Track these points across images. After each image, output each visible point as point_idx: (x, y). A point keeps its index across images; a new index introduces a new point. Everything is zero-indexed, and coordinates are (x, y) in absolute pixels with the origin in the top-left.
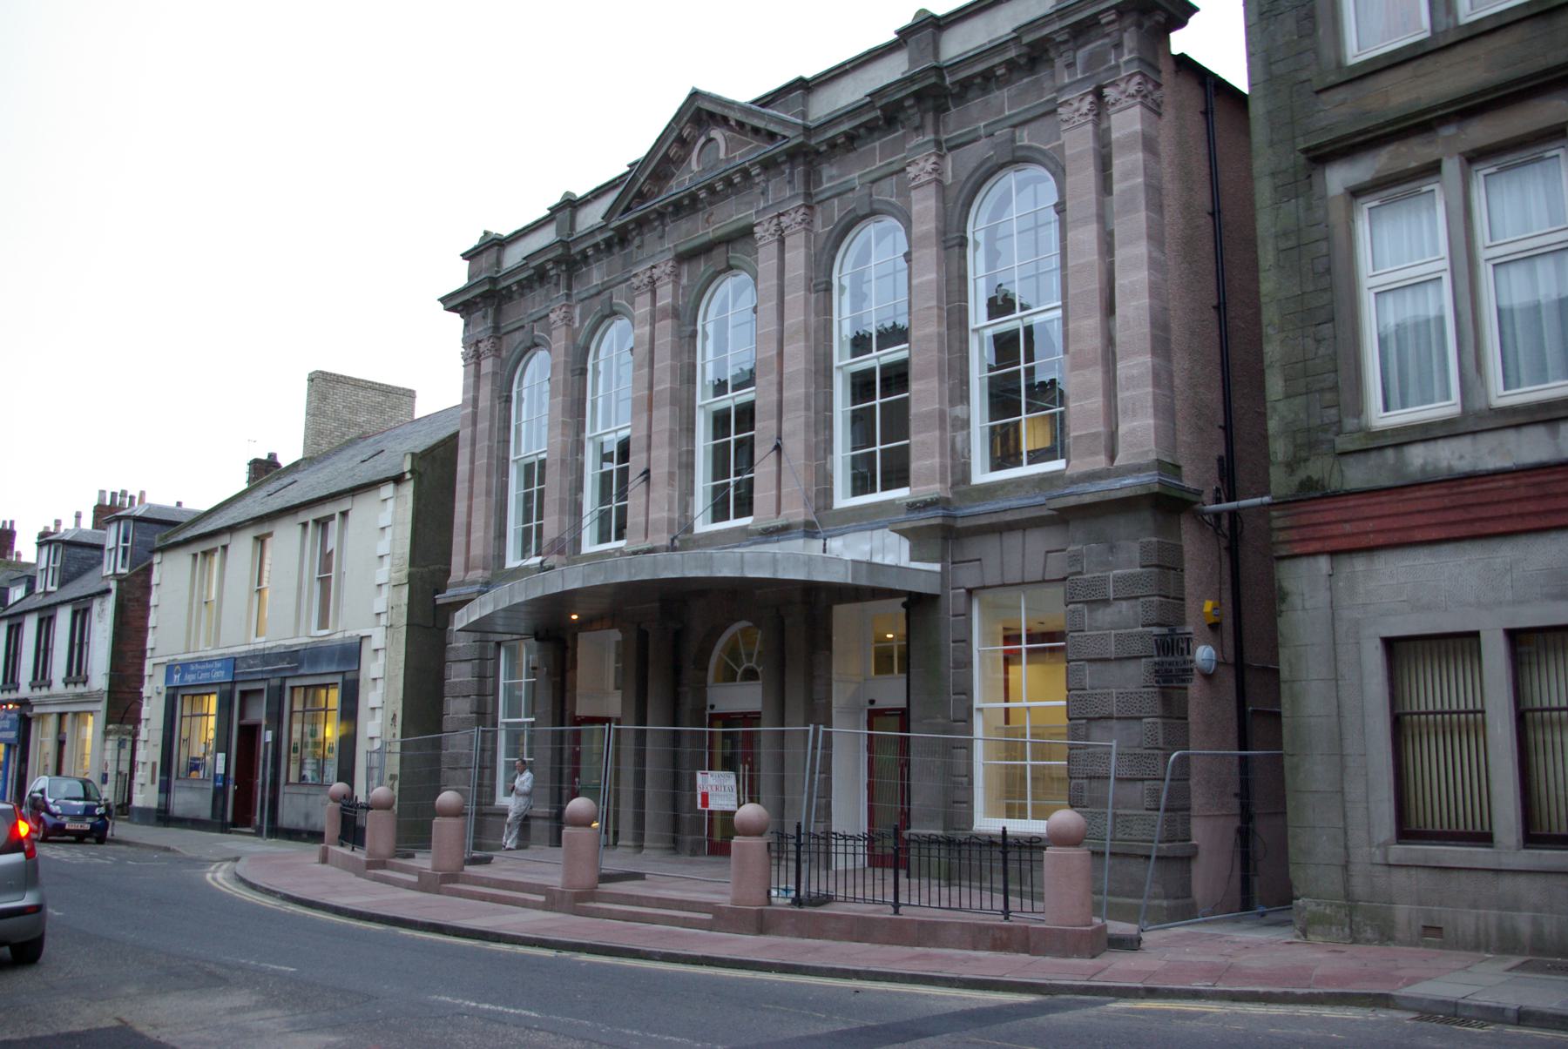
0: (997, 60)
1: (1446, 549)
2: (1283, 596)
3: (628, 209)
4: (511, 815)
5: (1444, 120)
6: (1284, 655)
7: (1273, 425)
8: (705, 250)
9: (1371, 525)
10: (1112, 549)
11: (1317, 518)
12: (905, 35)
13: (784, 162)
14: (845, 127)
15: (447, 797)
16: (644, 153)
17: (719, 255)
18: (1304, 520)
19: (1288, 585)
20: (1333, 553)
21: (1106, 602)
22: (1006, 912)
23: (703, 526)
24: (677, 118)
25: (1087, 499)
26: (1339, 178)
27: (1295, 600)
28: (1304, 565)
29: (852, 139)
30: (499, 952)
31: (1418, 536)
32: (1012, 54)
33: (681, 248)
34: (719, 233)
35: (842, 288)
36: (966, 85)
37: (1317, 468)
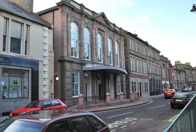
23: (102, 62)
26: (130, 55)
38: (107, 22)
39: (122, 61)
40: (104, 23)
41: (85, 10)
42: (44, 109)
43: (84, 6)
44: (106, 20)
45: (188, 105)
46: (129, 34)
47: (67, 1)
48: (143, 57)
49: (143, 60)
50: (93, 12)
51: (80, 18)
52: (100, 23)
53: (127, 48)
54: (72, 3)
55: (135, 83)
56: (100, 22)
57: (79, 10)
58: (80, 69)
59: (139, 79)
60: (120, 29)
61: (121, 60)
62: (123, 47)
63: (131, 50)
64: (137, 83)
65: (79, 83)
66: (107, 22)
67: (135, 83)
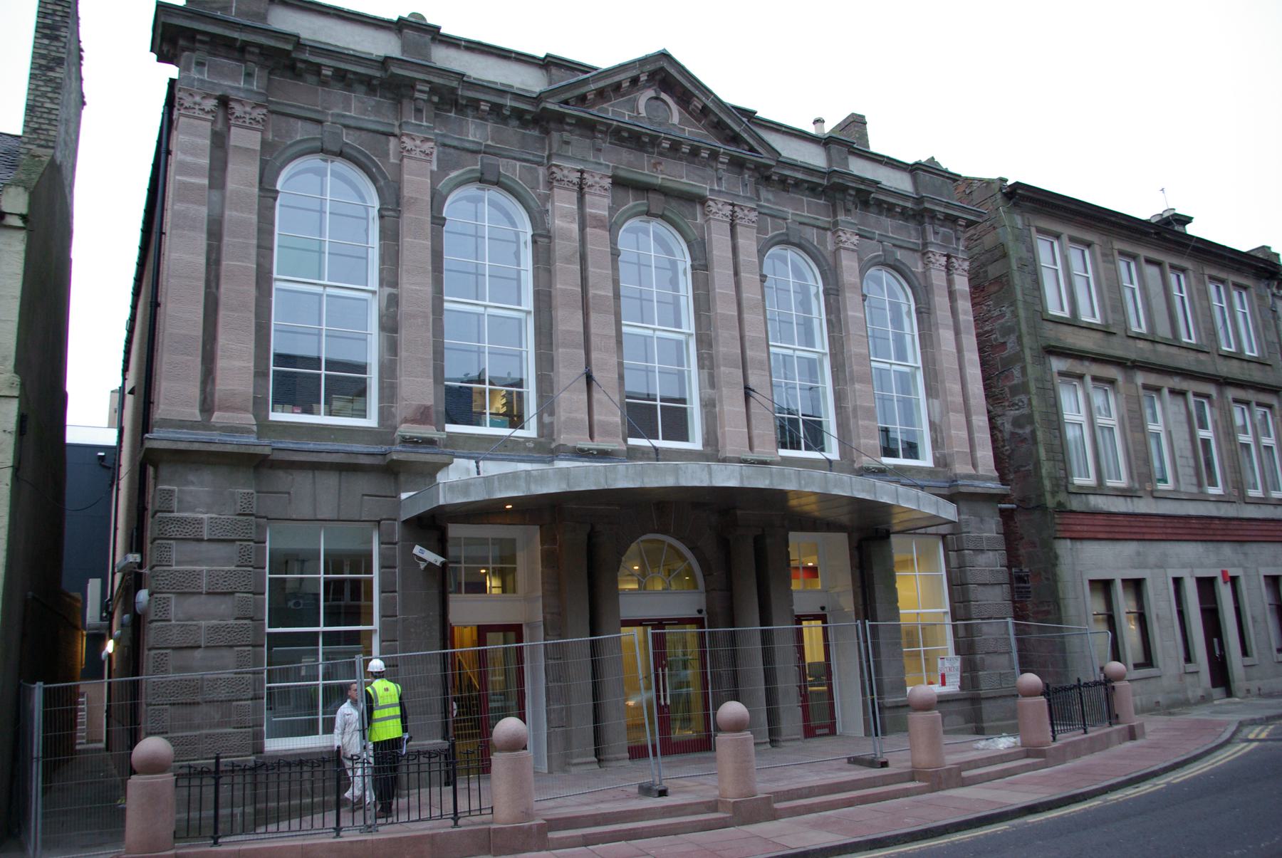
0: (901, 203)
1: (1264, 545)
2: (1056, 557)
3: (566, 102)
4: (678, 724)
5: (1087, 358)
6: (1060, 585)
7: (1044, 471)
8: (643, 188)
9: (1085, 528)
10: (982, 521)
11: (1071, 521)
12: (400, 26)
13: (749, 169)
14: (800, 176)
15: (151, 746)
16: (953, 169)
17: (656, 201)
18: (1066, 521)
19: (1059, 551)
20: (1071, 539)
21: (982, 551)
22: (338, 829)
23: (833, 452)
24: (643, 61)
25: (979, 490)
26: (1057, 364)
27: (1061, 560)
28: (1062, 542)
29: (798, 184)
30: (1126, 802)
31: (1117, 536)
32: (909, 205)
33: (622, 174)
34: (669, 184)
35: (817, 294)
36: (879, 203)
37: (1062, 497)
38: (719, 127)
39: (958, 418)
40: (693, 132)
41: (443, 57)
42: (551, 835)
43: (434, 33)
44: (705, 110)
45: (1086, 811)
46: (1028, 200)
47: (226, 9)
48: (1225, 369)
49: (1231, 393)
50: (549, 63)
51: (914, 240)
52: (634, 139)
53: (1015, 314)
54: (286, 21)
55: (1136, 586)
56: (648, 135)
57: (904, 196)
58: (373, 508)
59: (1189, 551)
60: (925, 171)
61: (946, 409)
62: (965, 305)
63: (1073, 322)
64: (1160, 602)
65: (376, 625)
66: (719, 127)
67: (1136, 586)
